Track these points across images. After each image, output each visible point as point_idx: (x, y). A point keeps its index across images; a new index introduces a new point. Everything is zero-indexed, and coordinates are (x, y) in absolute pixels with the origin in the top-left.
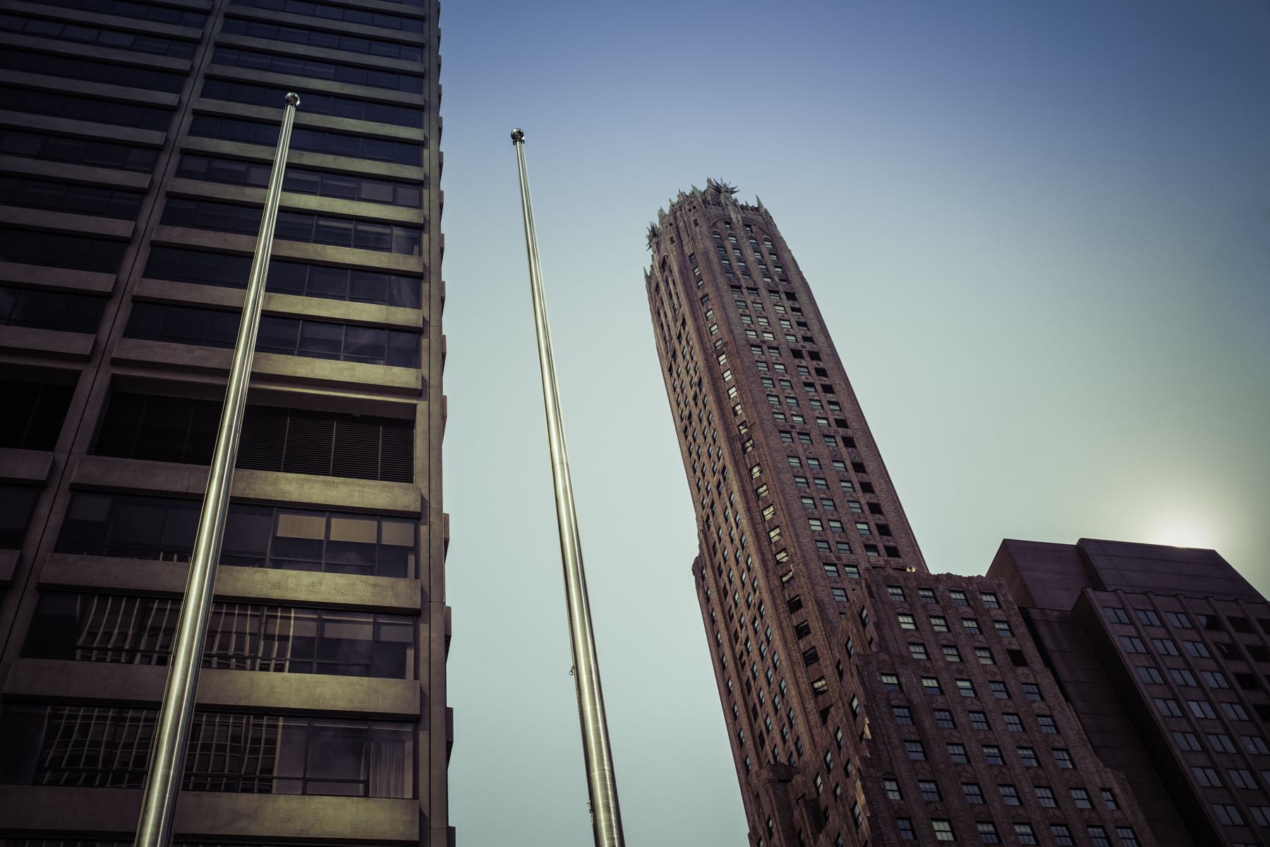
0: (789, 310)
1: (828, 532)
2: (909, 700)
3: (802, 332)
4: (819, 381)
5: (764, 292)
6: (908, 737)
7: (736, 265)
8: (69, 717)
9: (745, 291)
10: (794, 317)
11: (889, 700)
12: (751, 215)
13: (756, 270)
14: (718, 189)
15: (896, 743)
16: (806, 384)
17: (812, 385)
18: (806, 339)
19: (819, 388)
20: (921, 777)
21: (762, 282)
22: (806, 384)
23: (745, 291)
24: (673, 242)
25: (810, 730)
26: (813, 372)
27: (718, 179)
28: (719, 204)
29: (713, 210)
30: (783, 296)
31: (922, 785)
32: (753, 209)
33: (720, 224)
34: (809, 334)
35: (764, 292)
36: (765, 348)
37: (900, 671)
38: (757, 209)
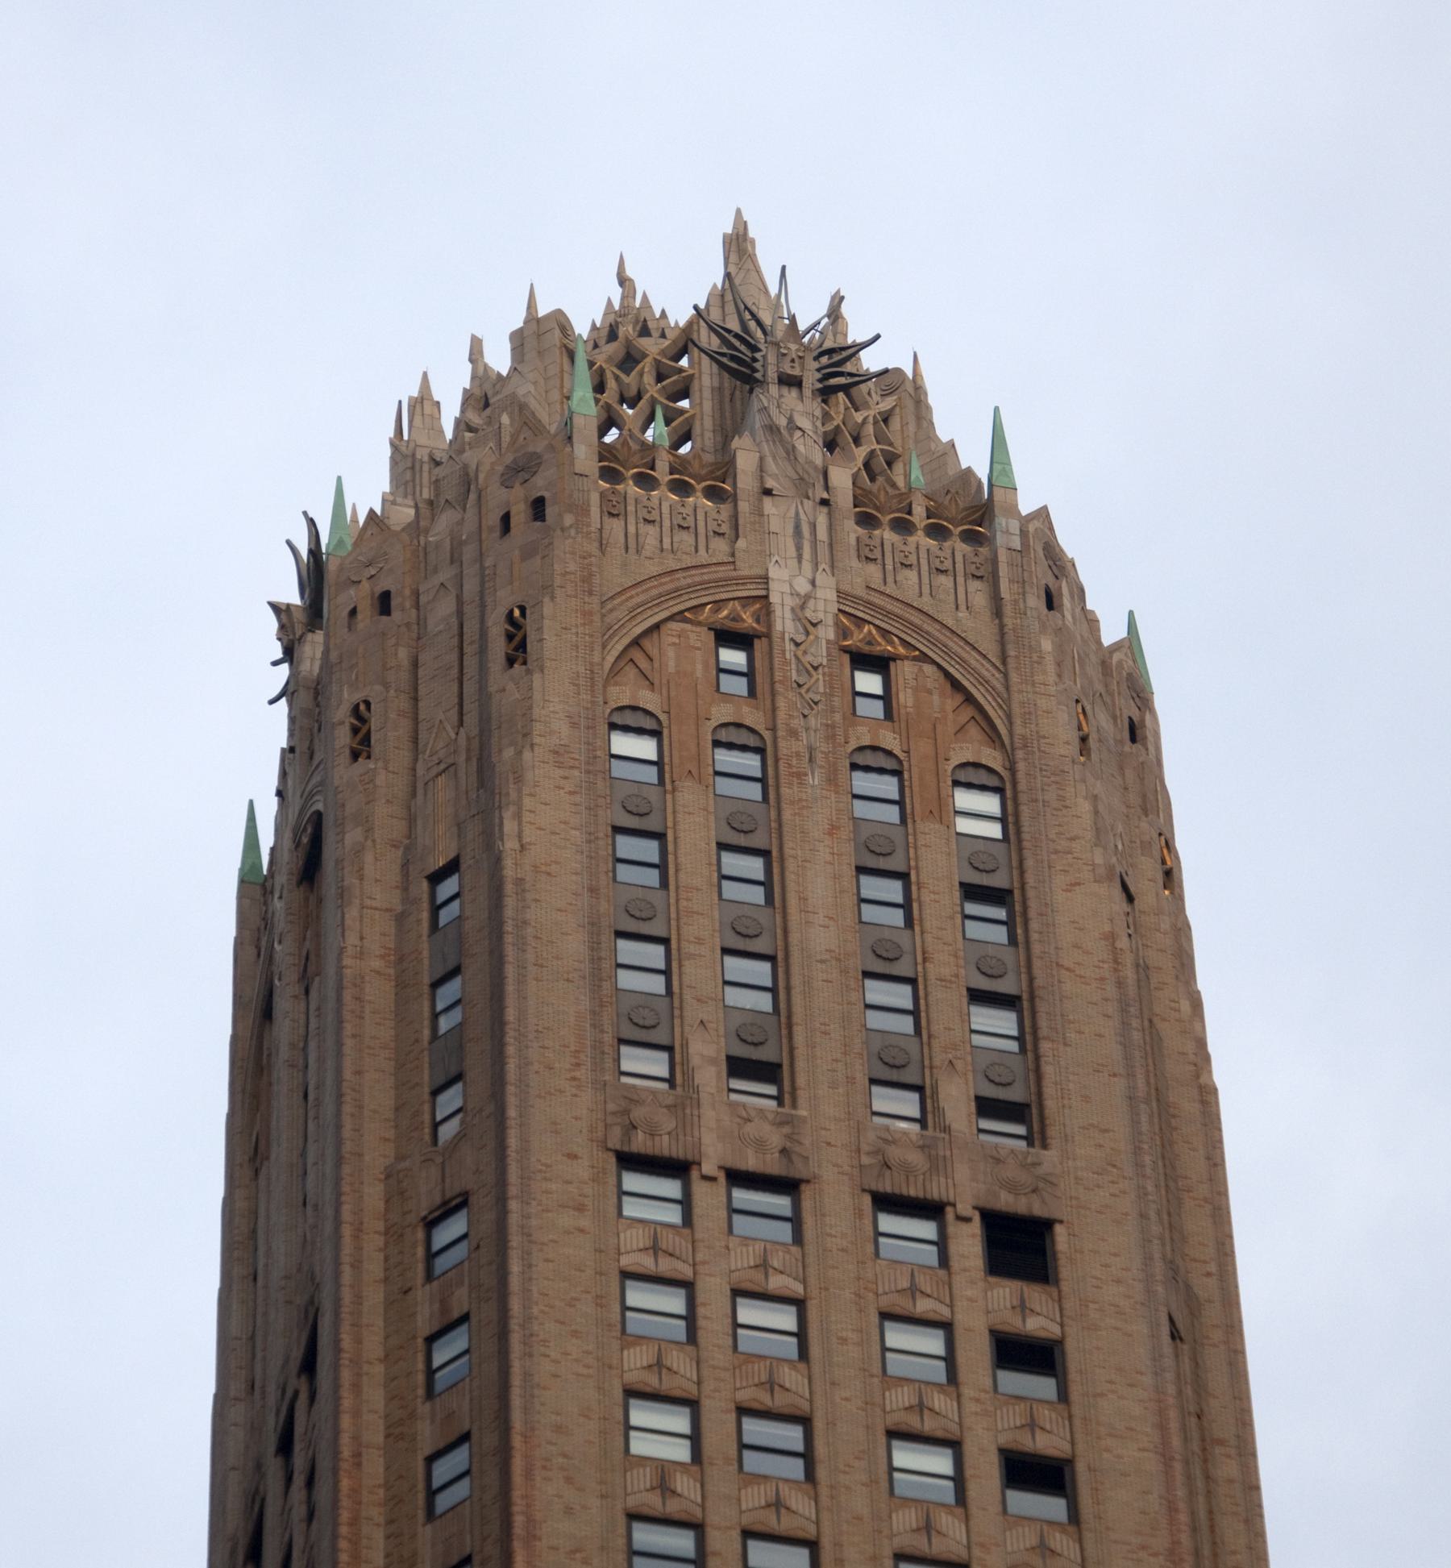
33: (684, 650)
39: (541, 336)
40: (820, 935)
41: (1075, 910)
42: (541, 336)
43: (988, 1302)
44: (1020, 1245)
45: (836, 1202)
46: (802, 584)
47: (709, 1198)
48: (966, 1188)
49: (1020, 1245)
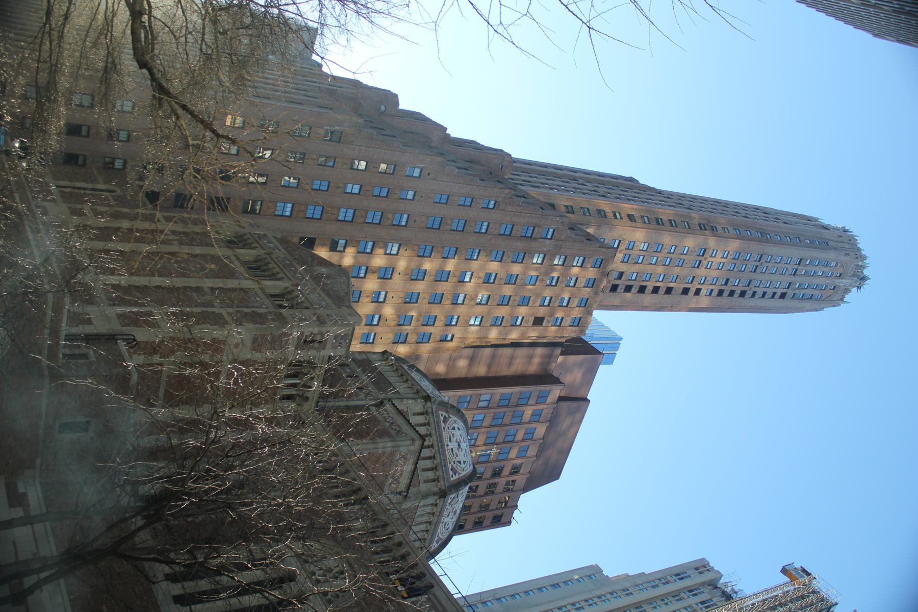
0: (775, 290)
1: (638, 253)
2: (535, 239)
3: (759, 293)
4: (727, 290)
5: (791, 279)
6: (515, 229)
7: (814, 269)
8: (383, 448)
9: (796, 267)
10: (770, 292)
11: (539, 226)
12: (840, 293)
13: (806, 281)
14: (864, 279)
15: (514, 219)
16: (727, 280)
17: (726, 283)
18: (754, 293)
19: (723, 288)
20: (491, 225)
21: (798, 281)
22: (727, 280)
23: (796, 267)
24: (839, 236)
25: (410, 485)
26: (734, 288)
27: (867, 286)
28: (854, 276)
29: (851, 270)
30: (784, 291)
31: (486, 224)
32: (843, 297)
33: (841, 270)
34: (756, 296)
35: (791, 279)
36: (758, 263)
37: (553, 242)
38: (842, 300)
41: (808, 304)
49: (783, 296)
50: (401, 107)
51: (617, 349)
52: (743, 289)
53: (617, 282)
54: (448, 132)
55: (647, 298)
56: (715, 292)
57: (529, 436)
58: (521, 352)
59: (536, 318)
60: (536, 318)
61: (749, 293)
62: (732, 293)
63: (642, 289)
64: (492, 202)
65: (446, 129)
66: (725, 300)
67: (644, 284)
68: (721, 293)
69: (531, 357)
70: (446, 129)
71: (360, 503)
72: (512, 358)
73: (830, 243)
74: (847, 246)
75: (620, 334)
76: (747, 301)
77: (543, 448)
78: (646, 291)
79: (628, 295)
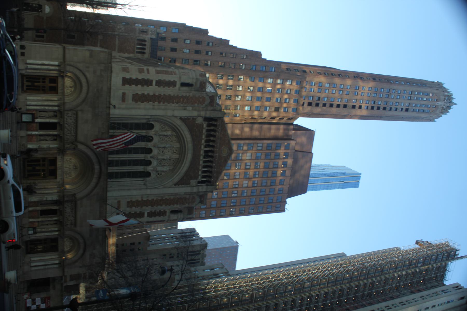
3: (394, 108)
16: (374, 102)
17: (374, 103)
22: (374, 102)
33: (436, 98)
34: (392, 110)
39: (452, 94)
40: (422, 102)
42: (452, 94)
43: (404, 108)
44: (407, 110)
45: (409, 101)
46: (439, 104)
47: (410, 95)
48: (410, 108)
49: (407, 110)
50: (209, 34)
51: (359, 179)
52: (384, 106)
53: (318, 102)
54: (230, 44)
55: (334, 110)
56: (370, 108)
57: (285, 164)
58: (273, 127)
59: (275, 108)
60: (275, 108)
61: (388, 108)
62: (379, 108)
63: (331, 106)
64: (245, 56)
65: (228, 41)
66: (375, 112)
67: (332, 103)
68: (372, 108)
69: (278, 129)
70: (228, 41)
71: (242, 301)
72: (270, 129)
73: (427, 85)
74: (437, 86)
75: (360, 172)
76: (388, 113)
77: (294, 172)
78: (334, 106)
79: (324, 108)
